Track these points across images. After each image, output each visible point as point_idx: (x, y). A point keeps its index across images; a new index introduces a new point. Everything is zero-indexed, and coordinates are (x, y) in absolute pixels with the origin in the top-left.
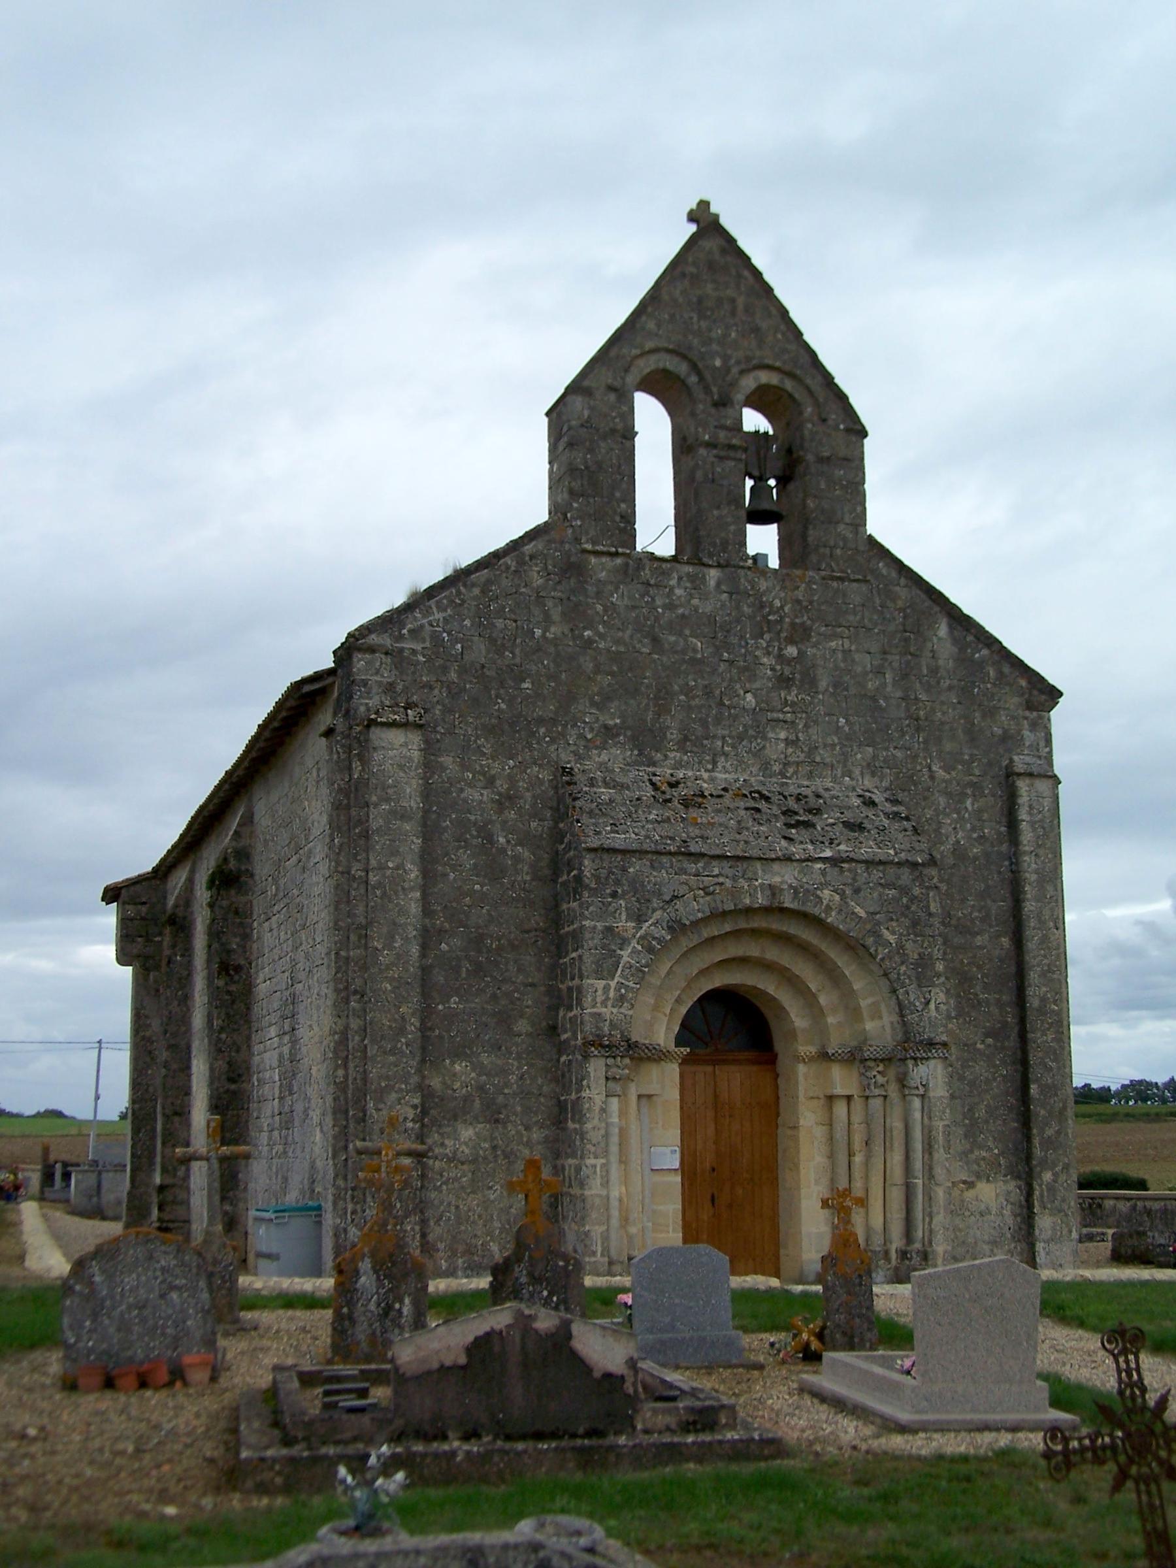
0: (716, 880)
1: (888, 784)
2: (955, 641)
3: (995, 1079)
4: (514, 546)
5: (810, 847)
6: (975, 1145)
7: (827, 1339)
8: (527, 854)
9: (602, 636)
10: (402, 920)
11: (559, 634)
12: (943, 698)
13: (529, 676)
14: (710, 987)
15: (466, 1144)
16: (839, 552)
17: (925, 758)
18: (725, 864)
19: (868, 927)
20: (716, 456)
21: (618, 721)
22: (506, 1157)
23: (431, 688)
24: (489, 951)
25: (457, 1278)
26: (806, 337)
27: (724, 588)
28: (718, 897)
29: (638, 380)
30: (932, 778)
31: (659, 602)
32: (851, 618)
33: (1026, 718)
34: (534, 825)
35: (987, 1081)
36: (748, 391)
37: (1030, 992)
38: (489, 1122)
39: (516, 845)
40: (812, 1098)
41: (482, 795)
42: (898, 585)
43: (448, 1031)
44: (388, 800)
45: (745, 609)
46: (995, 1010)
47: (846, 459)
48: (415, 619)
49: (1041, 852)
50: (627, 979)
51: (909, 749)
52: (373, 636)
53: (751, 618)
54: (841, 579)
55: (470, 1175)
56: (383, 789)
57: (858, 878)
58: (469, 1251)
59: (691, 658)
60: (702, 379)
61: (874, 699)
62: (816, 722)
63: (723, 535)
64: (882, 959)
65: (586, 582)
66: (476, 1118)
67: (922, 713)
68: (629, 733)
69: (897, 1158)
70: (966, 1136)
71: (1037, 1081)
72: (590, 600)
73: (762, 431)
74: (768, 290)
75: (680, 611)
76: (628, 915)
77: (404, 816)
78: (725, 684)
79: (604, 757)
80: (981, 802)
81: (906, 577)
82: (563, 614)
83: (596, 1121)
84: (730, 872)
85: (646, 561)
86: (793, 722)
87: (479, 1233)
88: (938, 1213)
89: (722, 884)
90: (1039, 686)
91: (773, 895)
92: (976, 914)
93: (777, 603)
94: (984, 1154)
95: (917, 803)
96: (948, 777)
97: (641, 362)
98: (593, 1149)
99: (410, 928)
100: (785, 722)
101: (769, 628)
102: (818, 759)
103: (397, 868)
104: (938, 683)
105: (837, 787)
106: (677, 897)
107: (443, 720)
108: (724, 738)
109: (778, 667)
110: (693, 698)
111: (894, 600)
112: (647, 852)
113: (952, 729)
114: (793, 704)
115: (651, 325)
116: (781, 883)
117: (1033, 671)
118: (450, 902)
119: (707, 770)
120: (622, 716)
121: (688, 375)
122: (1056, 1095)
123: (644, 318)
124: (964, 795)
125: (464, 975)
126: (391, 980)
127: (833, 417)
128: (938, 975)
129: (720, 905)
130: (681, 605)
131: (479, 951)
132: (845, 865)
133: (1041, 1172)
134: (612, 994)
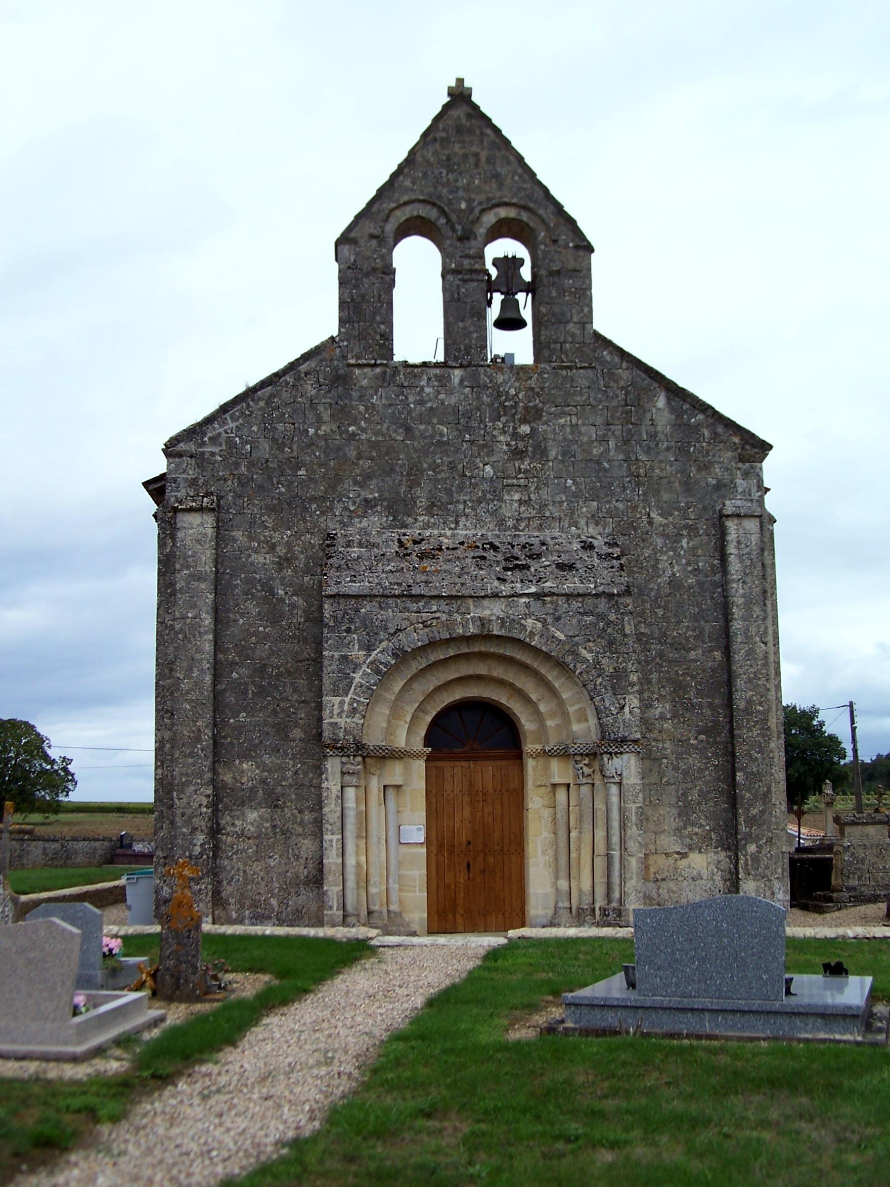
0: (434, 615)
1: (610, 530)
2: (672, 410)
4: (292, 367)
5: (519, 585)
6: (688, 823)
7: (159, 979)
8: (301, 601)
9: (363, 430)
10: (198, 656)
11: (328, 431)
12: (661, 458)
13: (304, 465)
14: (451, 700)
15: (252, 824)
17: (644, 508)
18: (442, 602)
19: (567, 647)
21: (376, 495)
22: (283, 833)
23: (226, 480)
24: (270, 677)
25: (244, 925)
26: (539, 177)
27: (466, 383)
28: (434, 629)
29: (396, 227)
30: (650, 523)
31: (411, 399)
32: (578, 398)
33: (739, 469)
34: (306, 579)
36: (489, 225)
37: (737, 695)
38: (270, 807)
39: (293, 595)
41: (265, 558)
44: (188, 567)
45: (485, 398)
47: (575, 271)
48: (214, 429)
50: (359, 696)
51: (630, 501)
52: (182, 444)
53: (490, 405)
54: (570, 368)
55: (255, 847)
58: (255, 904)
59: (438, 441)
60: (449, 221)
61: (599, 463)
62: (546, 485)
63: (467, 342)
64: (581, 673)
66: (260, 804)
67: (641, 471)
68: (385, 503)
69: (600, 833)
70: (680, 815)
71: (743, 769)
72: (354, 403)
73: (510, 256)
74: (507, 142)
75: (429, 405)
76: (360, 645)
77: (200, 578)
78: (467, 460)
79: (365, 523)
80: (696, 542)
81: (628, 362)
83: (333, 806)
84: (446, 609)
85: (401, 368)
86: (526, 486)
87: (262, 891)
88: (631, 878)
89: (438, 618)
90: (751, 441)
91: (483, 625)
93: (513, 392)
94: (696, 830)
96: (666, 522)
97: (398, 213)
98: (330, 828)
99: (205, 662)
100: (519, 486)
101: (504, 411)
102: (547, 514)
103: (195, 617)
104: (657, 445)
105: (564, 536)
106: (400, 630)
107: (235, 504)
108: (465, 502)
109: (513, 443)
111: (616, 381)
112: (376, 596)
113: (669, 482)
114: (526, 471)
115: (408, 183)
116: (491, 615)
117: (744, 429)
118: (240, 641)
119: (450, 529)
120: (380, 491)
121: (438, 218)
122: (762, 781)
123: (401, 178)
125: (250, 696)
126: (190, 702)
127: (564, 237)
128: (632, 685)
130: (430, 400)
131: (263, 678)
132: (548, 599)
133: (746, 844)
134: (346, 707)
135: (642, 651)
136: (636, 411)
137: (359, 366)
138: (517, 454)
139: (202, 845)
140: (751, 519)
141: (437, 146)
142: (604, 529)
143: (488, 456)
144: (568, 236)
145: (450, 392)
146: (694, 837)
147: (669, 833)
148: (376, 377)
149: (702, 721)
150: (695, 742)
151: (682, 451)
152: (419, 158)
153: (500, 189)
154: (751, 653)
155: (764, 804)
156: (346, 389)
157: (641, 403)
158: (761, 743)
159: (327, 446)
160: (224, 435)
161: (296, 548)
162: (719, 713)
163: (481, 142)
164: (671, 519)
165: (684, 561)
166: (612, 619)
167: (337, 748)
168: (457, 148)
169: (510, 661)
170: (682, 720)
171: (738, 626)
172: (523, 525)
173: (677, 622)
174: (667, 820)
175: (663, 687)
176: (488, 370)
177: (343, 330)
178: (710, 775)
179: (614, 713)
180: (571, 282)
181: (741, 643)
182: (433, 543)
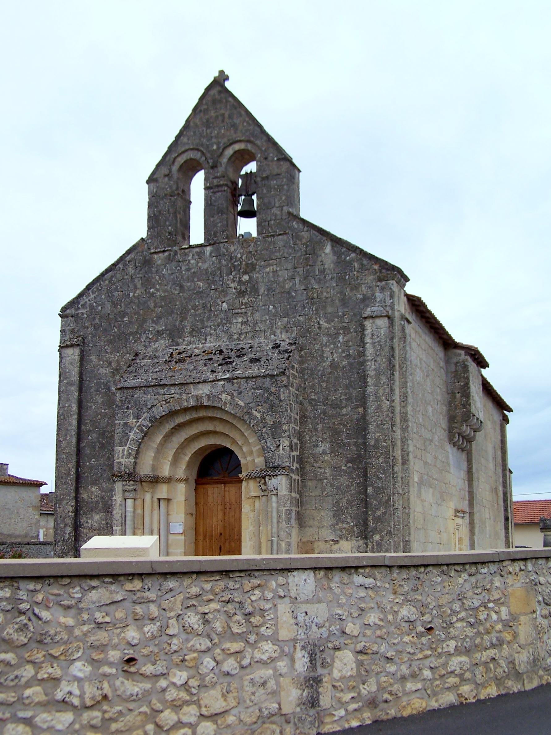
2: (334, 252)
3: (352, 485)
4: (122, 259)
9: (158, 290)
10: (70, 428)
11: (140, 293)
12: (327, 285)
14: (200, 447)
15: (96, 522)
16: (272, 222)
17: (316, 318)
18: (177, 388)
19: (245, 410)
20: (213, 192)
21: (164, 328)
23: (88, 328)
27: (213, 255)
30: (320, 328)
31: (183, 268)
32: (277, 254)
33: (378, 286)
35: (348, 486)
36: (229, 156)
40: (249, 498)
42: (303, 231)
43: (90, 474)
44: (66, 378)
46: (353, 448)
49: (378, 359)
52: (68, 310)
54: (273, 236)
56: (65, 374)
57: (241, 386)
61: (289, 293)
62: (257, 311)
63: (215, 229)
64: (253, 426)
65: (152, 267)
66: (100, 510)
68: (168, 332)
70: (334, 516)
71: (372, 485)
73: (249, 172)
75: (192, 271)
78: (213, 301)
81: (307, 227)
82: (142, 284)
83: (117, 510)
84: (179, 391)
86: (246, 313)
89: (173, 397)
90: (387, 267)
92: (343, 397)
94: (344, 525)
95: (310, 342)
96: (329, 326)
98: (116, 522)
100: (242, 313)
102: (257, 329)
104: (325, 277)
106: (153, 406)
109: (239, 287)
110: (197, 310)
111: (301, 240)
112: (142, 387)
113: (332, 300)
114: (246, 303)
119: (202, 343)
120: (166, 325)
122: (384, 493)
123: (182, 138)
124: (338, 334)
127: (271, 155)
128: (285, 432)
129: (173, 407)
131: (103, 439)
133: (373, 535)
134: (125, 453)
135: (312, 411)
136: (312, 257)
137: (155, 253)
138: (241, 293)
139: (69, 534)
140: (381, 318)
141: (202, 114)
142: (291, 334)
143: (224, 297)
144: (274, 154)
145: (204, 262)
146: (343, 530)
147: (327, 527)
148: (165, 258)
149: (350, 454)
150: (345, 468)
151: (341, 279)
152: (192, 124)
153: (235, 133)
154: (379, 407)
155: (386, 508)
156: (149, 267)
157: (316, 251)
158: (384, 467)
159: (139, 301)
160: (88, 302)
161: (122, 363)
162: (361, 449)
163: (226, 107)
164: (332, 324)
165: (340, 350)
166: (272, 391)
167: (119, 476)
168: (213, 114)
169: (212, 419)
170: (337, 454)
171: (371, 390)
172: (243, 337)
173: (335, 390)
174: (326, 519)
175: (325, 433)
176: (226, 244)
177: (149, 233)
178: (354, 490)
179: (273, 450)
180: (275, 182)
181: (372, 401)
182: (190, 352)
